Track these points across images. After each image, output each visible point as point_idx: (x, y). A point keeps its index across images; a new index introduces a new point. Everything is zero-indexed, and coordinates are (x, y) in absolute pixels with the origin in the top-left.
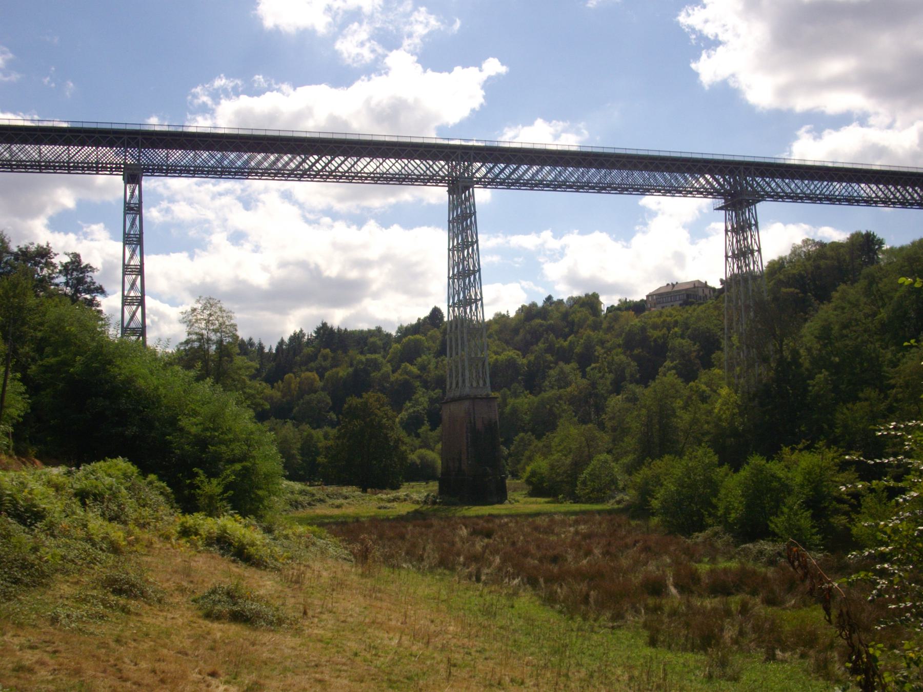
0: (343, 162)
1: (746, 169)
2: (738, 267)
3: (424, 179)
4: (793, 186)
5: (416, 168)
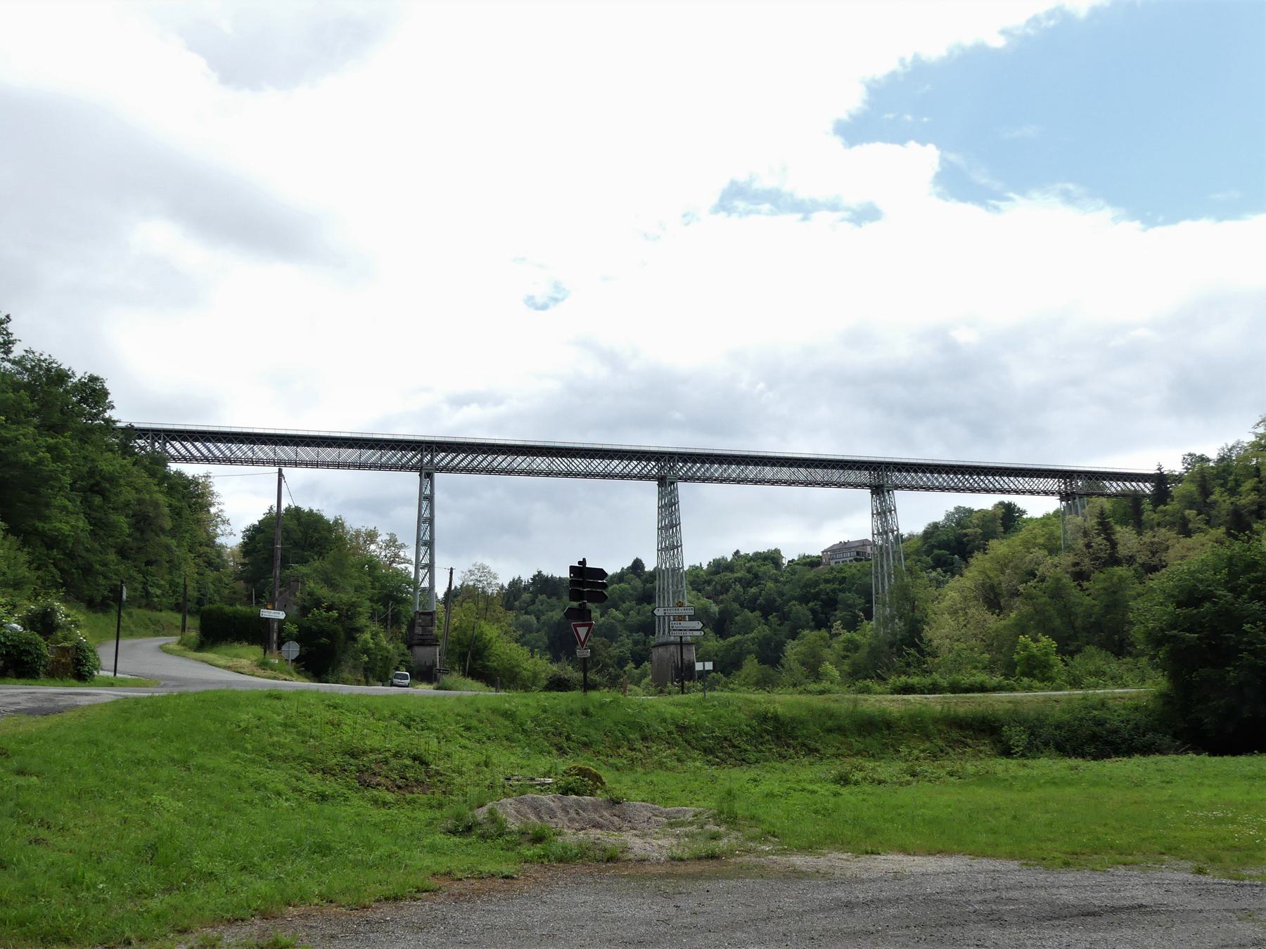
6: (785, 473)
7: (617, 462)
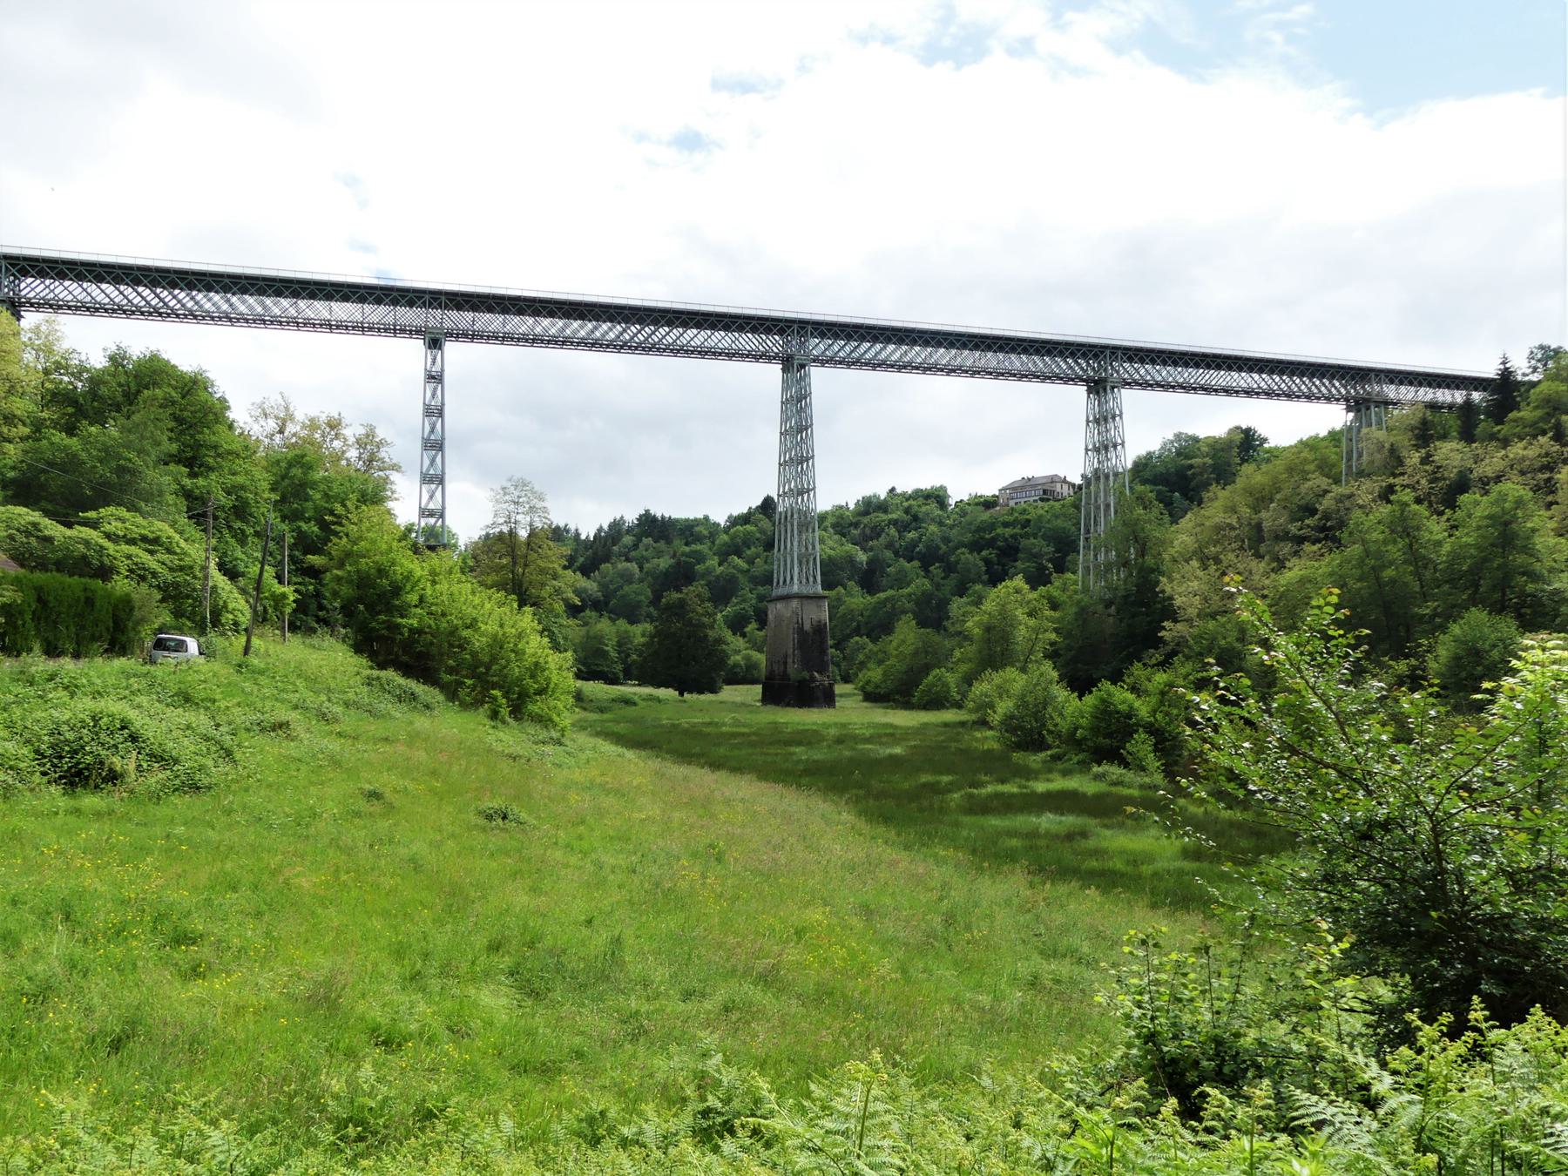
0: (668, 334)
1: (1113, 353)
2: (1099, 462)
4: (1164, 373)
7: (695, 331)
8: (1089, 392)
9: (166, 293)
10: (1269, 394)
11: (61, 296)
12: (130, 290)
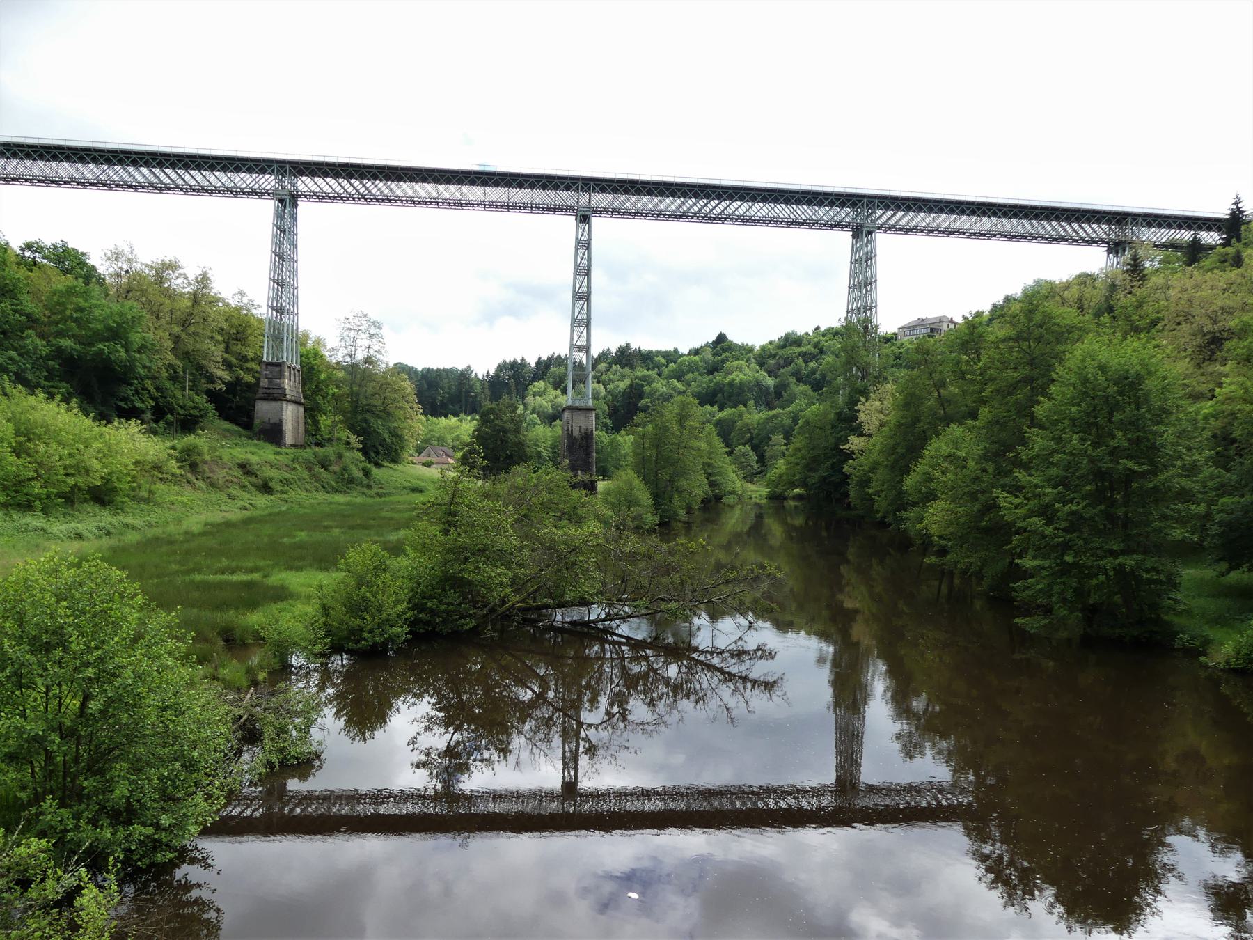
3: (810, 223)
5: (803, 213)
6: (670, 204)
7: (739, 203)
8: (1109, 252)
9: (358, 183)
10: (338, 197)
11: (263, 186)
12: (346, 182)
